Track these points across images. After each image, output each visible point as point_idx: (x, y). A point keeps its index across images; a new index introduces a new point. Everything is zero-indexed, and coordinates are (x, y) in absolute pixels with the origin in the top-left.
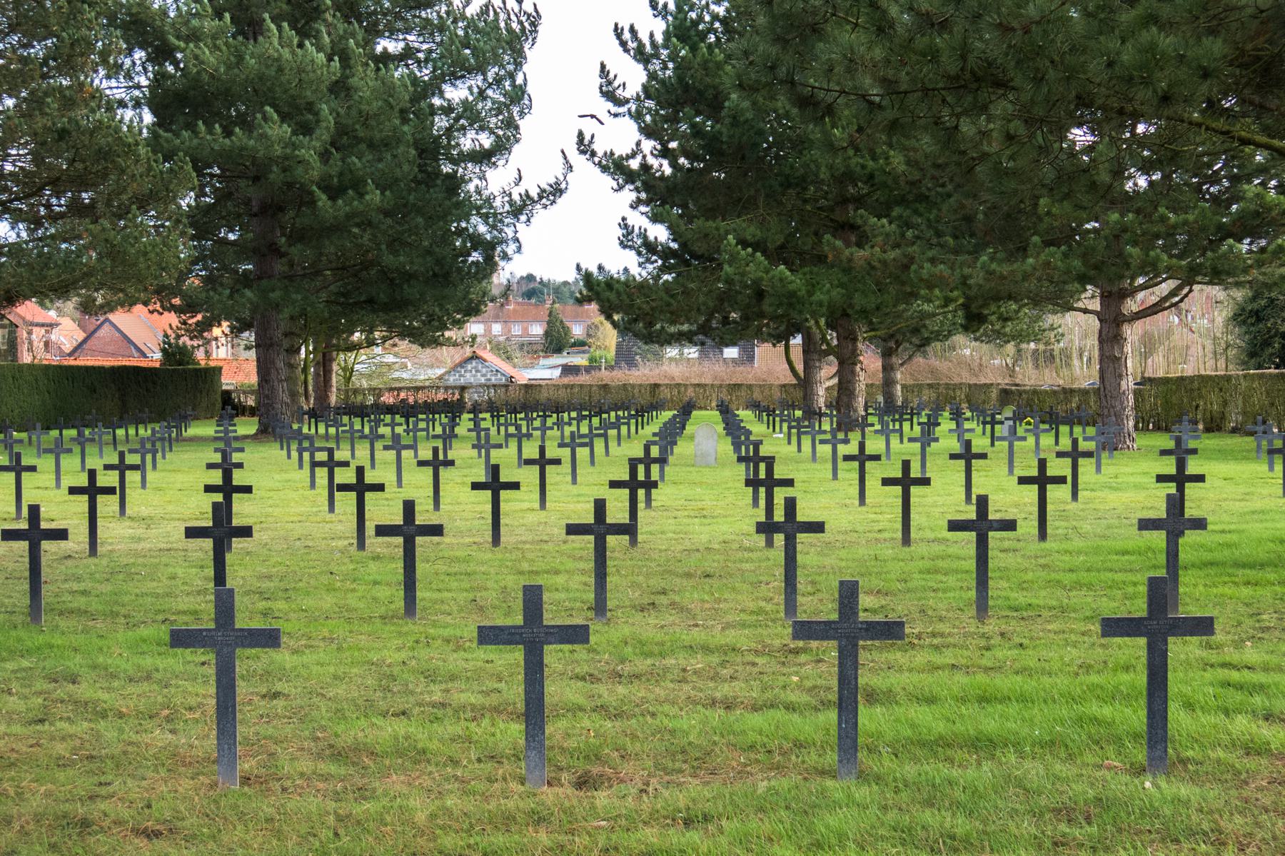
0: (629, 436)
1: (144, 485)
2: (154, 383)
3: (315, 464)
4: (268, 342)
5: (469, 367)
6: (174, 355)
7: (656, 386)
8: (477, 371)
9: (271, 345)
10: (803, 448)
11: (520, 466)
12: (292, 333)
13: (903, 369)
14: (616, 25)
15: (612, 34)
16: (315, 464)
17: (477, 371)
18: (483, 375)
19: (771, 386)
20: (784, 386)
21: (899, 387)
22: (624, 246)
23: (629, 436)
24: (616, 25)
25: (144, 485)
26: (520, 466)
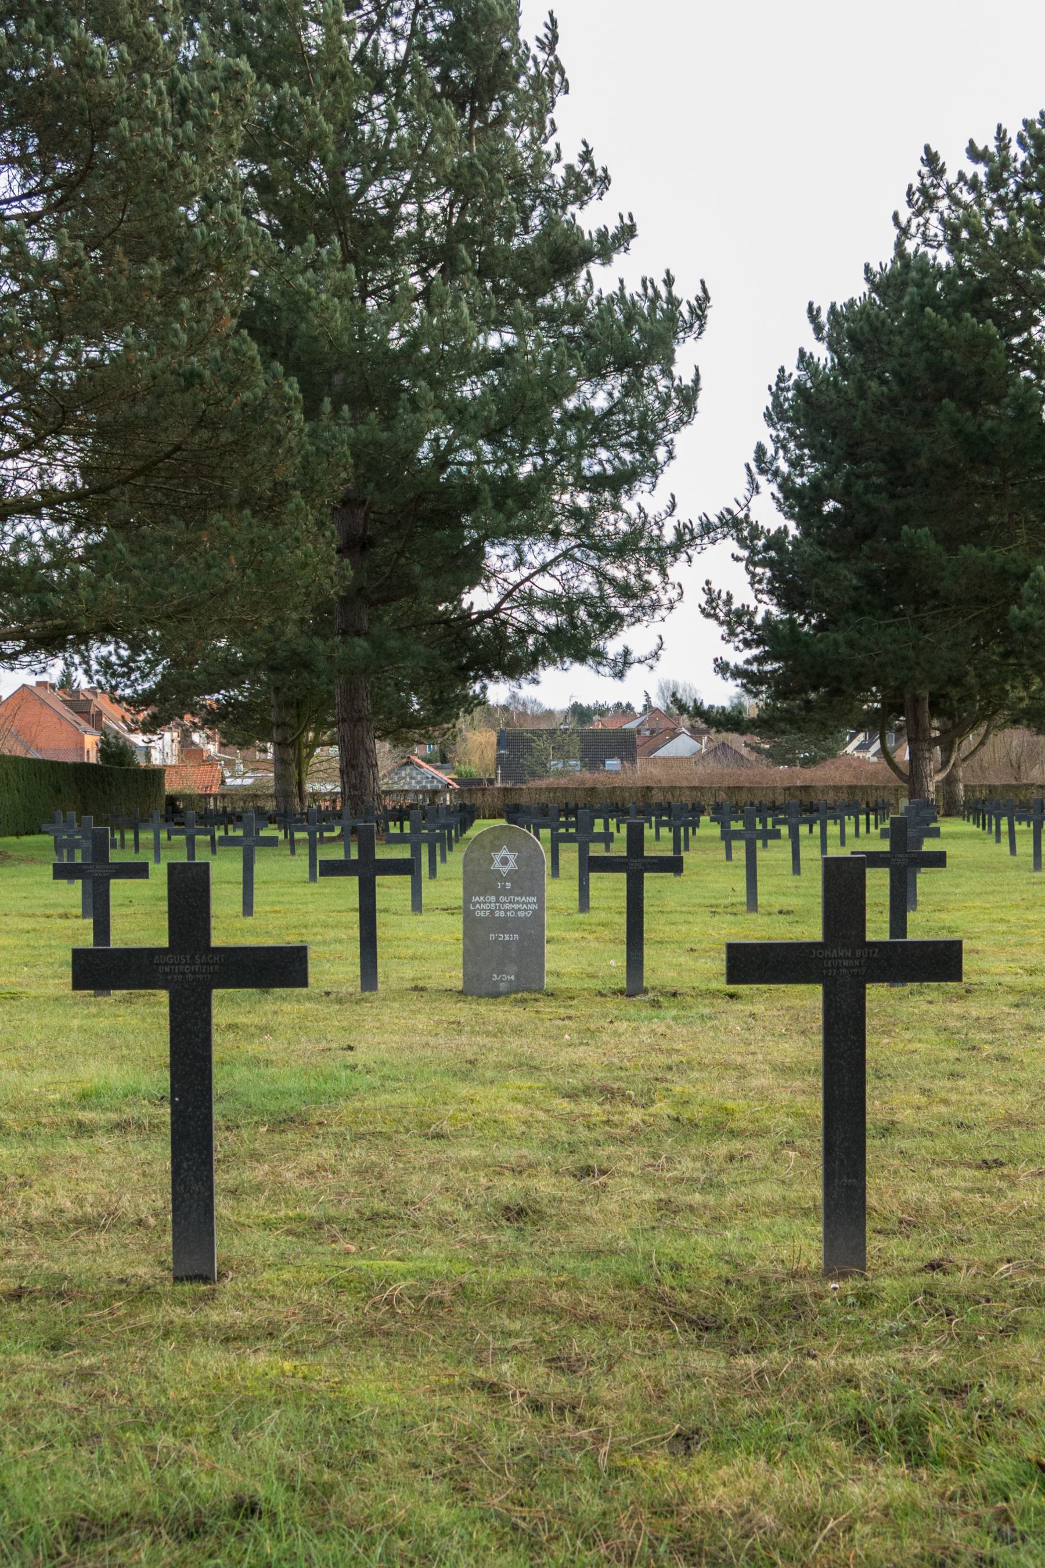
0: (857, 834)
1: (417, 905)
2: (110, 784)
3: (591, 865)
4: (356, 715)
5: (403, 774)
6: (112, 755)
7: (649, 789)
8: (412, 778)
9: (360, 719)
10: (734, 855)
11: (313, 878)
12: (285, 724)
13: (965, 765)
14: (811, 304)
15: (806, 315)
16: (591, 865)
17: (412, 778)
18: (418, 783)
19: (774, 788)
20: (789, 788)
21: (961, 786)
22: (708, 615)
23: (857, 834)
24: (811, 304)
25: (417, 905)
26: (313, 878)
